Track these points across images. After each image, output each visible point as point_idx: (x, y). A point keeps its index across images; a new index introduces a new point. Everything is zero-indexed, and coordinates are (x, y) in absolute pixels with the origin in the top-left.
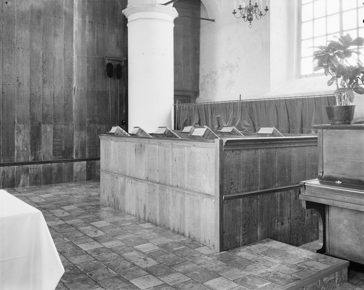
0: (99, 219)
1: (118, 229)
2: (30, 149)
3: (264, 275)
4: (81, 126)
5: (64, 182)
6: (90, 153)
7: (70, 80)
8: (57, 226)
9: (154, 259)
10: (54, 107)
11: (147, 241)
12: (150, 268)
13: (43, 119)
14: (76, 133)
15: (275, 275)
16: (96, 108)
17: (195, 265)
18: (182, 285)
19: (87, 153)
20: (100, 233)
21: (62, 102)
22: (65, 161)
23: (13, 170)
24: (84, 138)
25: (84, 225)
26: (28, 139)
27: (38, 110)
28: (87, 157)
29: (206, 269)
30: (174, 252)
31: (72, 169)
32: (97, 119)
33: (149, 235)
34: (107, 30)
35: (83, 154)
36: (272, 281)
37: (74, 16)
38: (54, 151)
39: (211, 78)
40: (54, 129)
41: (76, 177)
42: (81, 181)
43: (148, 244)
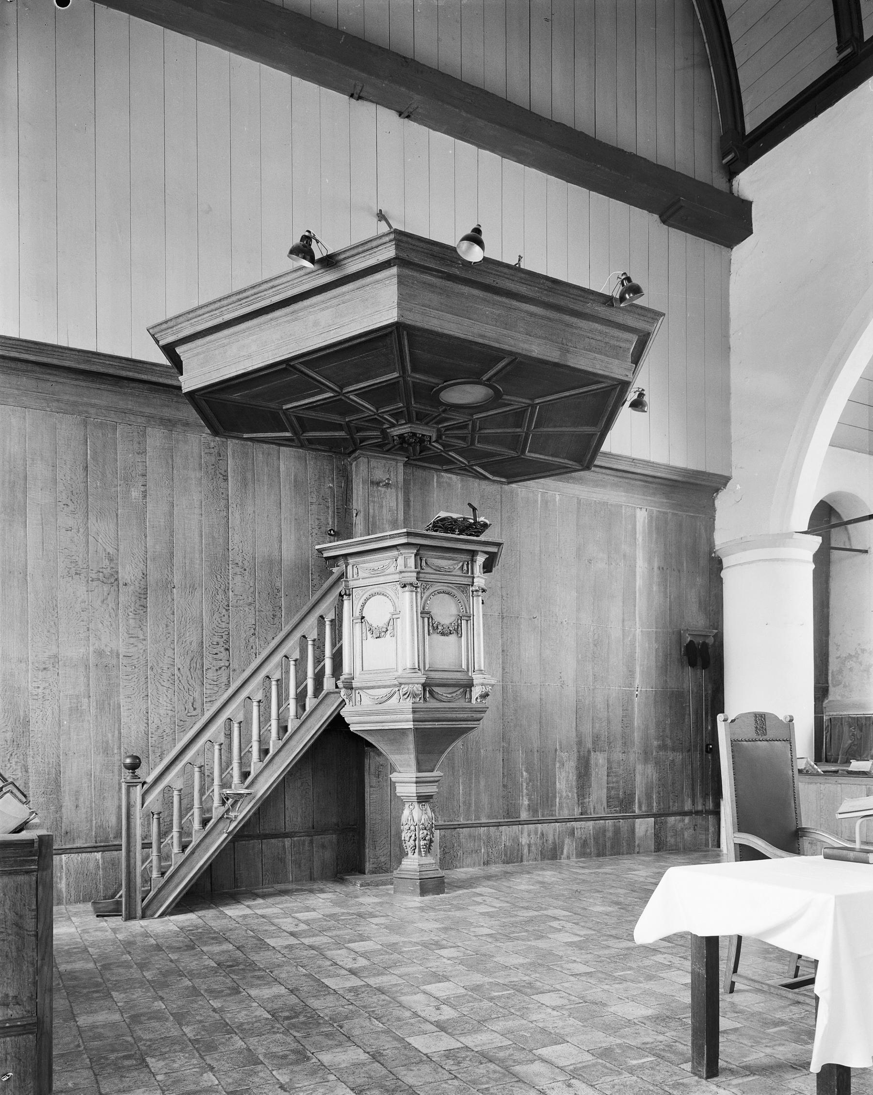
0: (362, 938)
1: (395, 956)
2: (575, 795)
3: (778, 1042)
4: (646, 755)
5: (623, 854)
6: (659, 803)
7: (631, 673)
8: (286, 948)
9: (454, 1007)
10: (609, 722)
11: (446, 978)
12: (444, 1022)
13: (593, 743)
14: (639, 768)
15: (759, 1042)
16: (668, 722)
17: (524, 1022)
18: (496, 1050)
19: (655, 804)
20: (362, 962)
21: (619, 712)
22: (624, 818)
23: (555, 830)
24: (650, 776)
25: (333, 947)
26: (573, 777)
27: (587, 729)
28: (655, 810)
29: (543, 1030)
30: (491, 999)
31: (633, 831)
32: (669, 742)
33: (450, 968)
34: (684, 581)
35: (649, 805)
36: (658, 1056)
37: (637, 561)
38: (609, 797)
39: (861, 663)
40: (609, 761)
41: (638, 846)
42: (647, 853)
43: (446, 984)
